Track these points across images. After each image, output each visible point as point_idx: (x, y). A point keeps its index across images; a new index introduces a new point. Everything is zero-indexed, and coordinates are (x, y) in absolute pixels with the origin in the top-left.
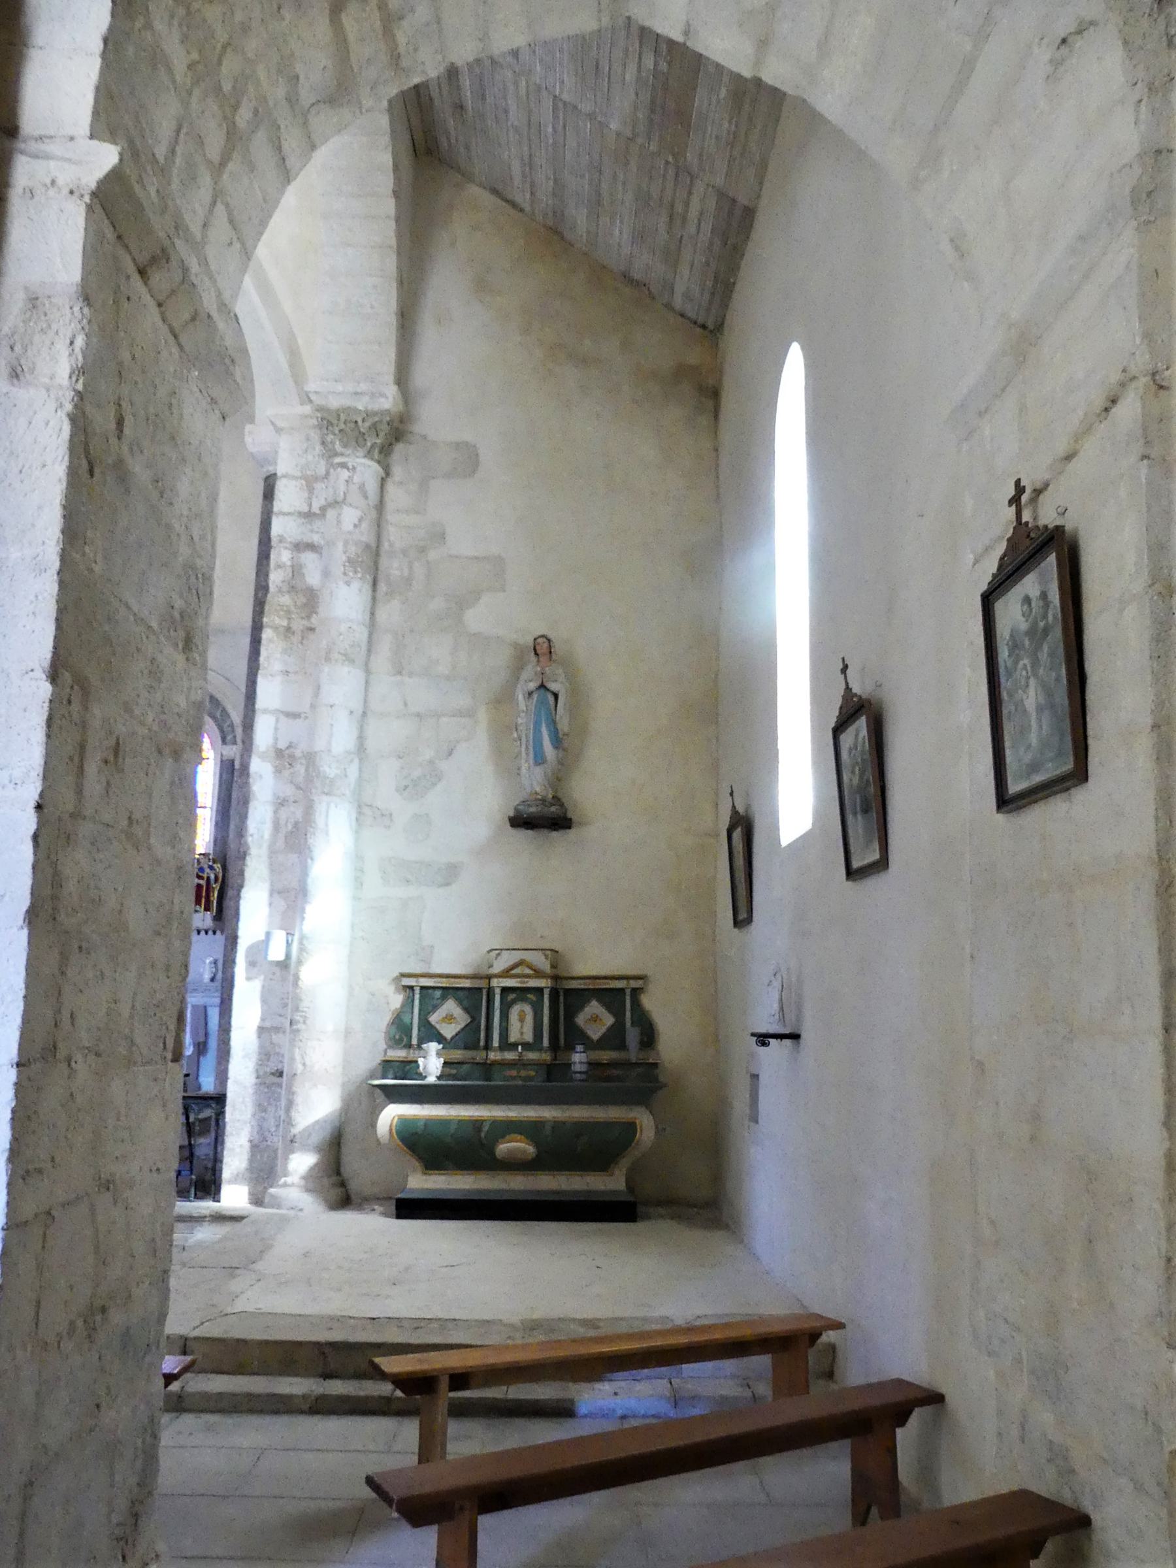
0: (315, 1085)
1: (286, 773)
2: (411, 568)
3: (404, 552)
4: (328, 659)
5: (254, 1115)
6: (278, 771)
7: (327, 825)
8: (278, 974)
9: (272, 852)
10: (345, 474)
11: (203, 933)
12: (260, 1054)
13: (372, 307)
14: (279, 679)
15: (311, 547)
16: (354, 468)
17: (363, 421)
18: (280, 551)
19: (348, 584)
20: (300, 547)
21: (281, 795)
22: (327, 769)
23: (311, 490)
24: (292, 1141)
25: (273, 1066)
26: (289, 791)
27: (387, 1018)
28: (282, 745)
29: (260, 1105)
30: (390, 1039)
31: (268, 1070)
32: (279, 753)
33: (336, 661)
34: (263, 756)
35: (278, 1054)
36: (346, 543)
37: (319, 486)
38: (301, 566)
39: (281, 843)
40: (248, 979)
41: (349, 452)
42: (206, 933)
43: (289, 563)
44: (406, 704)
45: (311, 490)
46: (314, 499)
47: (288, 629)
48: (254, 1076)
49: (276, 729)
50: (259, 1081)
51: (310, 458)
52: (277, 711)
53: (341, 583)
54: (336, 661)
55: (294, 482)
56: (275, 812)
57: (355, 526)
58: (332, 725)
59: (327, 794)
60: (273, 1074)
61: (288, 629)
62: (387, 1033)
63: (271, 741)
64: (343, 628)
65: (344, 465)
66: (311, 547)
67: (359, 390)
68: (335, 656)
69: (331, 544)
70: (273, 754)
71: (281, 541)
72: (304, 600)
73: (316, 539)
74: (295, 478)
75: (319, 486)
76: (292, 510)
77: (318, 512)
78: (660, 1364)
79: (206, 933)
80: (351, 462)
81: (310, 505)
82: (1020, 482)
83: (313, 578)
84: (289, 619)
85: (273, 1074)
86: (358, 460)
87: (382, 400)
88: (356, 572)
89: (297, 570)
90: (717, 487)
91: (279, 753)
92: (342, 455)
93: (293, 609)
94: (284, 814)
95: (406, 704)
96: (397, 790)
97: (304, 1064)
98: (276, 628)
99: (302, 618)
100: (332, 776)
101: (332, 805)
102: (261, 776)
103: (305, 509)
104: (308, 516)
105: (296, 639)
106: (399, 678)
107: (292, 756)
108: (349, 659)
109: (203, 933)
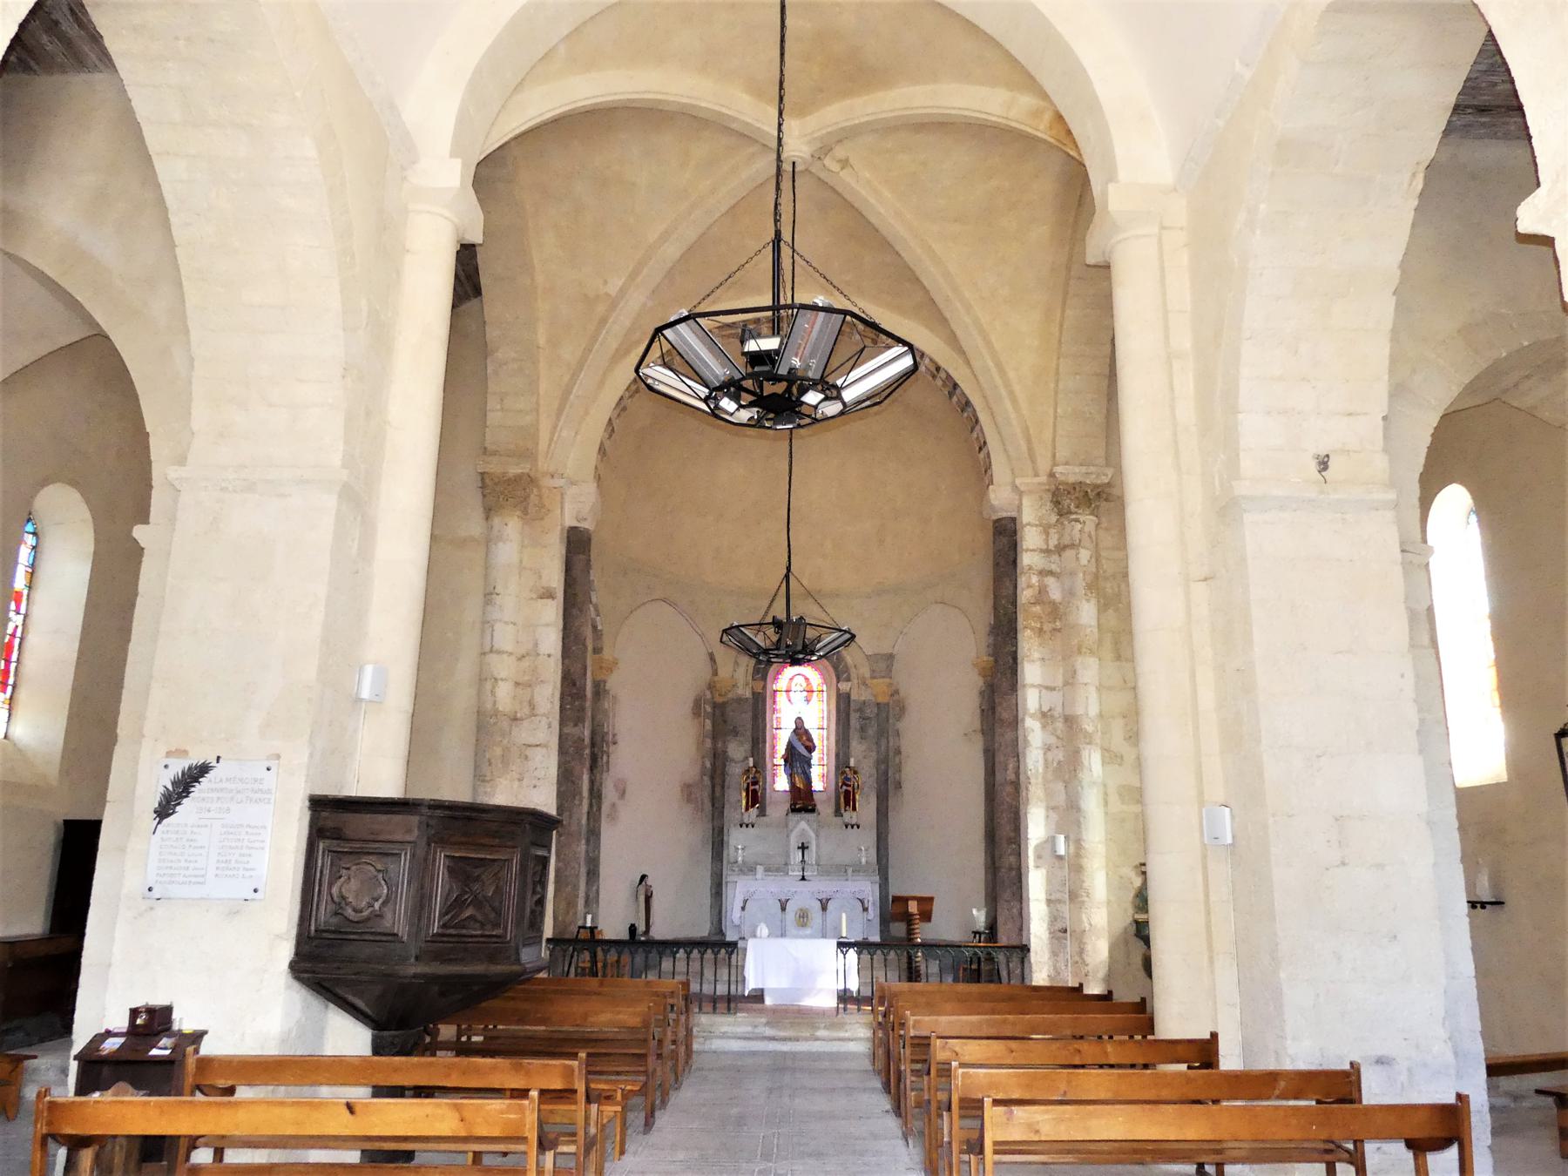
0: (1099, 938)
1: (1050, 728)
2: (1119, 587)
3: (1114, 576)
4: (1080, 652)
5: (1049, 959)
6: (1044, 727)
7: (1090, 764)
8: (1057, 864)
9: (1046, 781)
10: (1079, 526)
11: (849, 827)
12: (1050, 917)
13: (1090, 413)
14: (1038, 663)
15: (1051, 573)
16: (1084, 522)
17: (1092, 491)
18: (1030, 576)
19: (1088, 601)
20: (1043, 573)
21: (1048, 743)
22: (1087, 727)
23: (1047, 534)
24: (1086, 975)
25: (1059, 925)
26: (1053, 740)
27: (1132, 894)
28: (1045, 709)
29: (1053, 952)
30: (1136, 907)
31: (1056, 928)
32: (1044, 715)
33: (1085, 653)
34: (1032, 716)
35: (1062, 917)
36: (1084, 573)
37: (1052, 531)
38: (1046, 586)
39: (1050, 776)
40: (1037, 867)
41: (1081, 511)
42: (852, 827)
43: (1037, 584)
44: (1125, 682)
45: (1047, 534)
46: (1050, 541)
47: (1041, 630)
48: (1047, 932)
49: (1040, 697)
50: (1051, 935)
51: (1044, 512)
52: (1039, 686)
53: (1084, 601)
54: (1085, 653)
55: (1035, 528)
56: (1045, 754)
57: (1089, 561)
58: (1087, 697)
59: (1088, 744)
60: (1060, 931)
61: (1041, 630)
62: (1133, 902)
63: (1037, 706)
64: (1089, 630)
65: (1077, 520)
66: (1051, 573)
67: (1089, 471)
68: (1084, 650)
69: (1073, 574)
70: (1040, 716)
71: (1030, 569)
72: (1050, 610)
73: (1054, 567)
74: (1036, 526)
75: (1052, 531)
76: (1035, 547)
77: (1053, 549)
78: (1545, 1070)
79: (852, 827)
80: (1082, 519)
81: (1048, 546)
82: (635, 929)
83: (1055, 594)
84: (1041, 622)
85: (1060, 931)
86: (1088, 517)
87: (1103, 477)
88: (1092, 593)
89: (1043, 590)
90: (704, 299)
91: (1044, 715)
92: (1076, 513)
93: (1042, 615)
94: (1050, 756)
95: (1125, 682)
96: (1125, 739)
97: (1091, 925)
98: (1032, 629)
99: (1050, 622)
100: (1091, 731)
101: (1092, 751)
102: (1033, 731)
103: (1045, 547)
104: (1047, 552)
105: (1047, 636)
106: (1118, 663)
107: (1052, 716)
108: (1092, 652)
109: (849, 827)
